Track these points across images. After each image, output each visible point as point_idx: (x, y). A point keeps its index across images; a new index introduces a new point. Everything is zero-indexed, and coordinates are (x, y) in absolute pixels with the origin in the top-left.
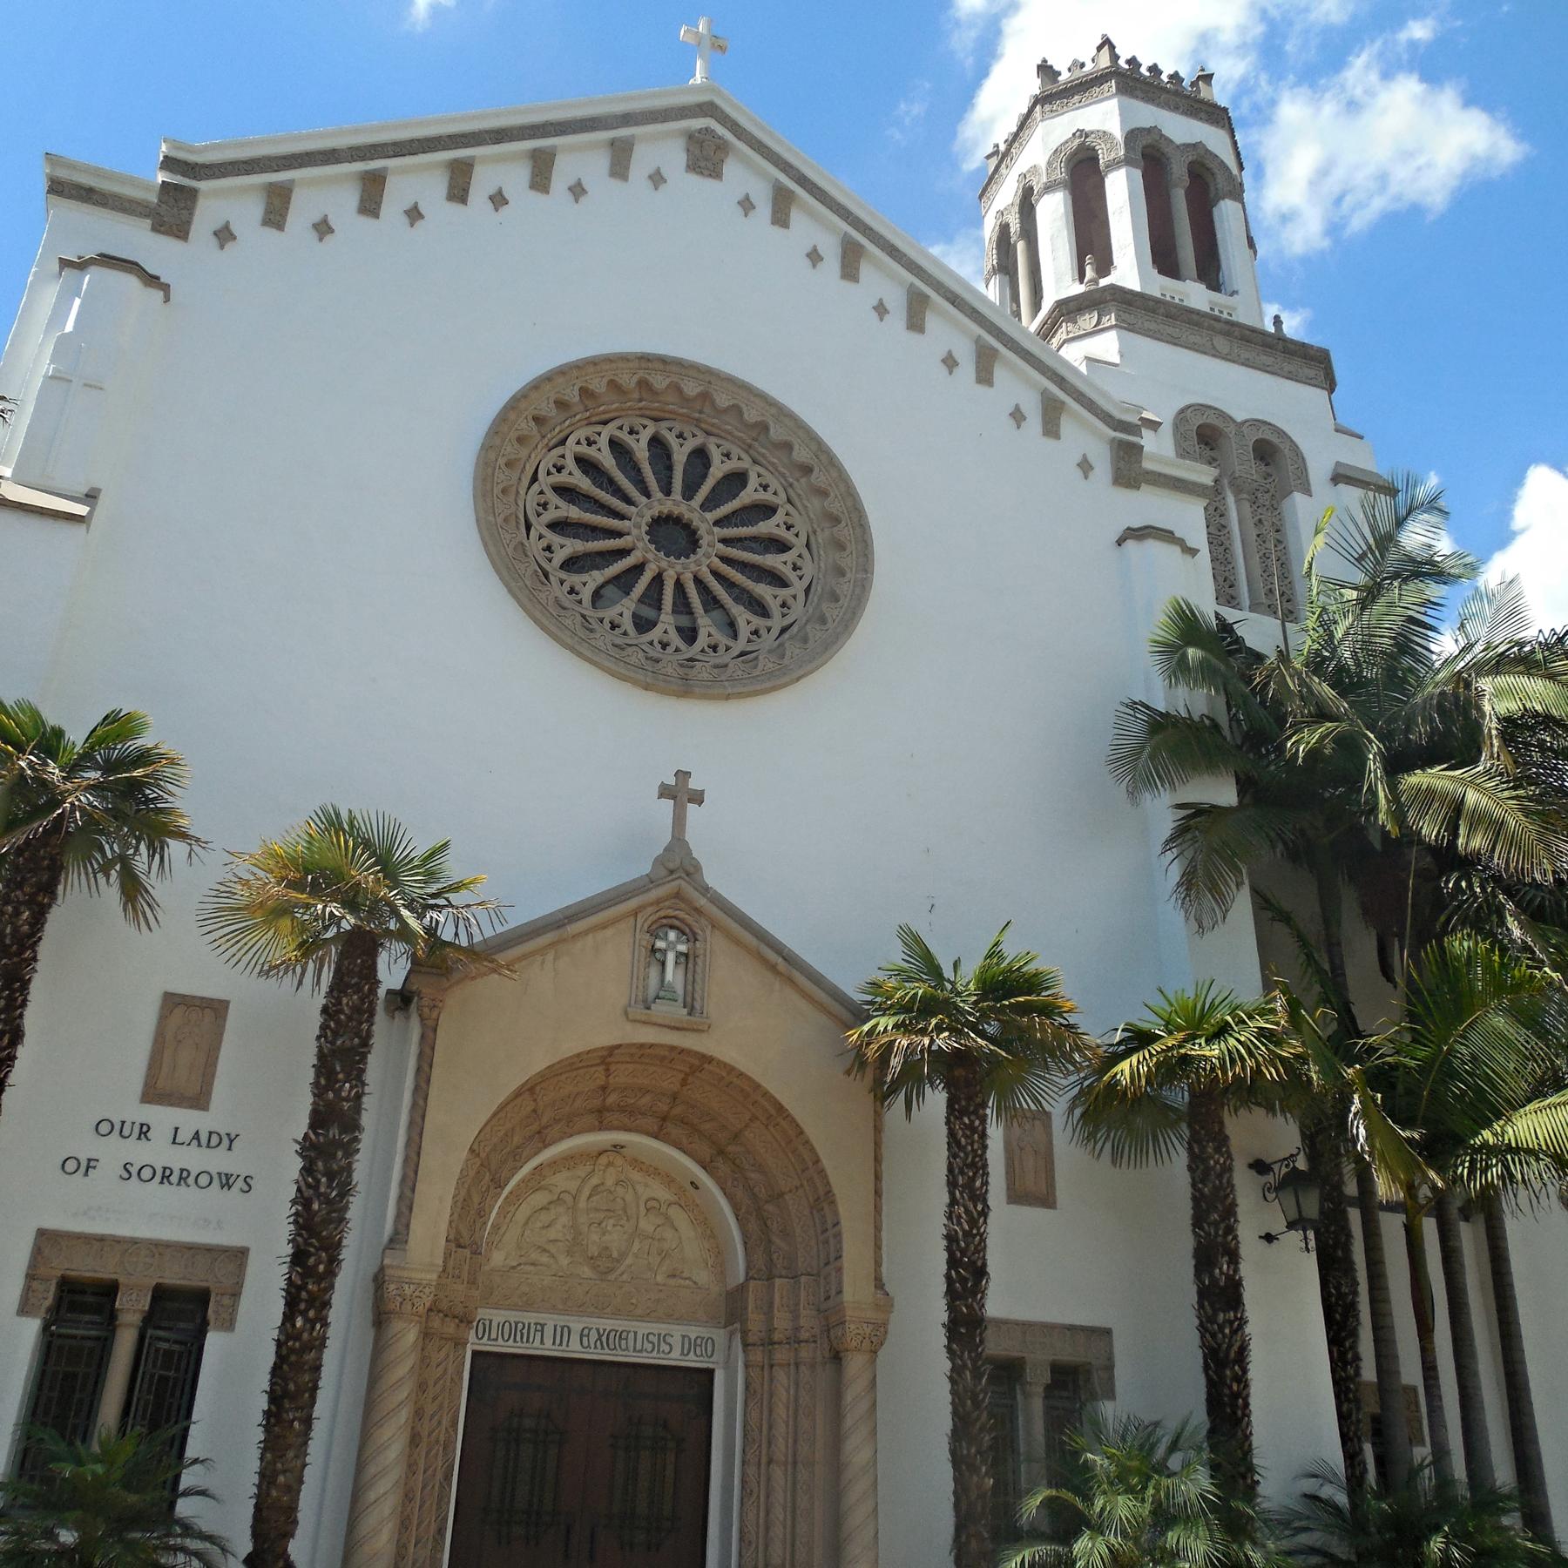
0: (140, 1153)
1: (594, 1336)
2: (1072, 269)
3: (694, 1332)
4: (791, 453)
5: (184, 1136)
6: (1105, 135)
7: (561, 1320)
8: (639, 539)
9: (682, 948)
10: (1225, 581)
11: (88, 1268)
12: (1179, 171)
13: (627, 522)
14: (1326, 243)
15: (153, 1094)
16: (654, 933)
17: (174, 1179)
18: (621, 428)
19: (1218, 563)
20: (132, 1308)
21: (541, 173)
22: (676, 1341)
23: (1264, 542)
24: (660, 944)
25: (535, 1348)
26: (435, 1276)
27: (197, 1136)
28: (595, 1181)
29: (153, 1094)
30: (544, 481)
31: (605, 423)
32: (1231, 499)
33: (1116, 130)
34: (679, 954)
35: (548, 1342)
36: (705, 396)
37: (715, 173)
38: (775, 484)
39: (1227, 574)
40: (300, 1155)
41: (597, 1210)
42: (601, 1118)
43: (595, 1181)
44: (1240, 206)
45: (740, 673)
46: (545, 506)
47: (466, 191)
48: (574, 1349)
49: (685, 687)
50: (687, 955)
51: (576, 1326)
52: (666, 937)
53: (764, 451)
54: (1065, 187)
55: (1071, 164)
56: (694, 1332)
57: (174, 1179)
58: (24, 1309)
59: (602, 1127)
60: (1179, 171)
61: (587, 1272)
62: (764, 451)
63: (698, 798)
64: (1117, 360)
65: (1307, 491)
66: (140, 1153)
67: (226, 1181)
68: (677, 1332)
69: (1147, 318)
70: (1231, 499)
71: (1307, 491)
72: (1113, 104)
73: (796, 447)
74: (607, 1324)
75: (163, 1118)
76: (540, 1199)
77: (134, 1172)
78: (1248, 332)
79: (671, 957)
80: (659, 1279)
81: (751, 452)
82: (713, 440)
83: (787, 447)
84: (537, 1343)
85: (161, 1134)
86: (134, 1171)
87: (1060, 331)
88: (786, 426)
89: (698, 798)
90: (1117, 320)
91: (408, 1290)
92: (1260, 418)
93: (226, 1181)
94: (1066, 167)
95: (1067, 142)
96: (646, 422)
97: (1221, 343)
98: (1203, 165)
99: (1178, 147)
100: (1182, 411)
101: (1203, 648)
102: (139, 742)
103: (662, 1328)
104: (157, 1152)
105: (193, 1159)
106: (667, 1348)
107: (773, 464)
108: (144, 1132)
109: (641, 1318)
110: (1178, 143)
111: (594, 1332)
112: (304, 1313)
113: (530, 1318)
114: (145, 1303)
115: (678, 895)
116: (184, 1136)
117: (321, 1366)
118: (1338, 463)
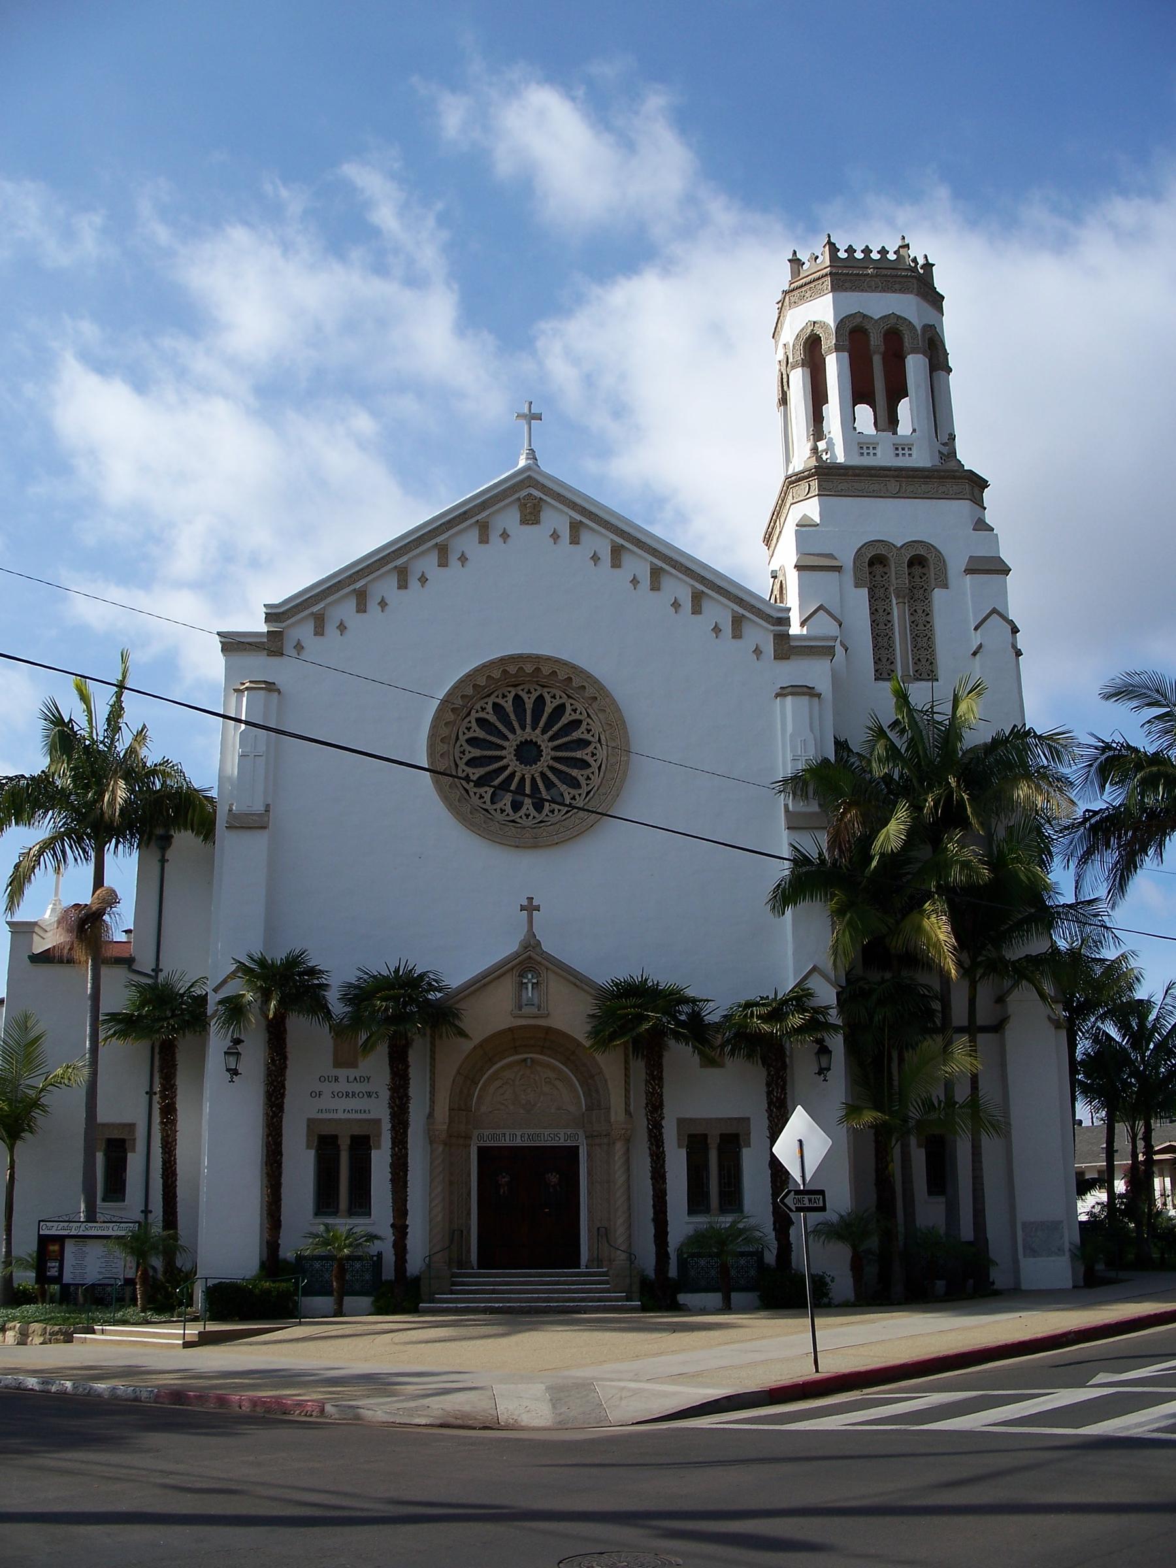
0: (336, 1087)
1: (526, 1136)
3: (569, 1132)
5: (351, 1079)
6: (824, 325)
7: (512, 1131)
8: (511, 760)
9: (535, 981)
11: (327, 1131)
12: (876, 340)
13: (505, 760)
14: (294, 1261)
15: (338, 1064)
16: (521, 976)
17: (350, 1096)
18: (497, 697)
20: (344, 1144)
21: (443, 553)
22: (562, 1136)
24: (525, 981)
25: (502, 1143)
26: (446, 1127)
27: (355, 1078)
28: (521, 1073)
29: (338, 1064)
30: (462, 738)
31: (489, 696)
33: (830, 319)
34: (533, 984)
35: (507, 1139)
36: (538, 670)
37: (537, 522)
38: (580, 708)
40: (389, 1089)
41: (523, 1085)
42: (516, 1050)
43: (521, 1073)
45: (562, 829)
46: (463, 753)
47: (406, 581)
48: (518, 1142)
49: (535, 845)
50: (537, 983)
51: (519, 1134)
52: (527, 978)
54: (803, 366)
55: (807, 346)
56: (569, 1132)
57: (350, 1096)
58: (308, 1147)
59: (517, 1053)
60: (876, 340)
61: (522, 1111)
63: (538, 909)
64: (819, 522)
66: (336, 1087)
67: (369, 1095)
68: (562, 1132)
69: (840, 481)
71: (946, 586)
72: (828, 299)
74: (531, 1131)
75: (342, 1073)
76: (498, 1083)
77: (336, 1094)
79: (530, 986)
80: (553, 1111)
82: (546, 690)
84: (503, 1141)
85: (342, 1079)
86: (336, 1094)
89: (538, 909)
91: (437, 1133)
93: (369, 1095)
95: (803, 329)
96: (509, 689)
97: (893, 486)
99: (876, 321)
102: (326, 993)
103: (556, 1131)
104: (343, 1086)
105: (357, 1087)
106: (558, 1139)
108: (336, 1079)
109: (545, 1128)
110: (876, 318)
111: (526, 1135)
112: (398, 1147)
113: (498, 1131)
114: (348, 1142)
115: (530, 957)
116: (351, 1079)
117: (750, 1133)
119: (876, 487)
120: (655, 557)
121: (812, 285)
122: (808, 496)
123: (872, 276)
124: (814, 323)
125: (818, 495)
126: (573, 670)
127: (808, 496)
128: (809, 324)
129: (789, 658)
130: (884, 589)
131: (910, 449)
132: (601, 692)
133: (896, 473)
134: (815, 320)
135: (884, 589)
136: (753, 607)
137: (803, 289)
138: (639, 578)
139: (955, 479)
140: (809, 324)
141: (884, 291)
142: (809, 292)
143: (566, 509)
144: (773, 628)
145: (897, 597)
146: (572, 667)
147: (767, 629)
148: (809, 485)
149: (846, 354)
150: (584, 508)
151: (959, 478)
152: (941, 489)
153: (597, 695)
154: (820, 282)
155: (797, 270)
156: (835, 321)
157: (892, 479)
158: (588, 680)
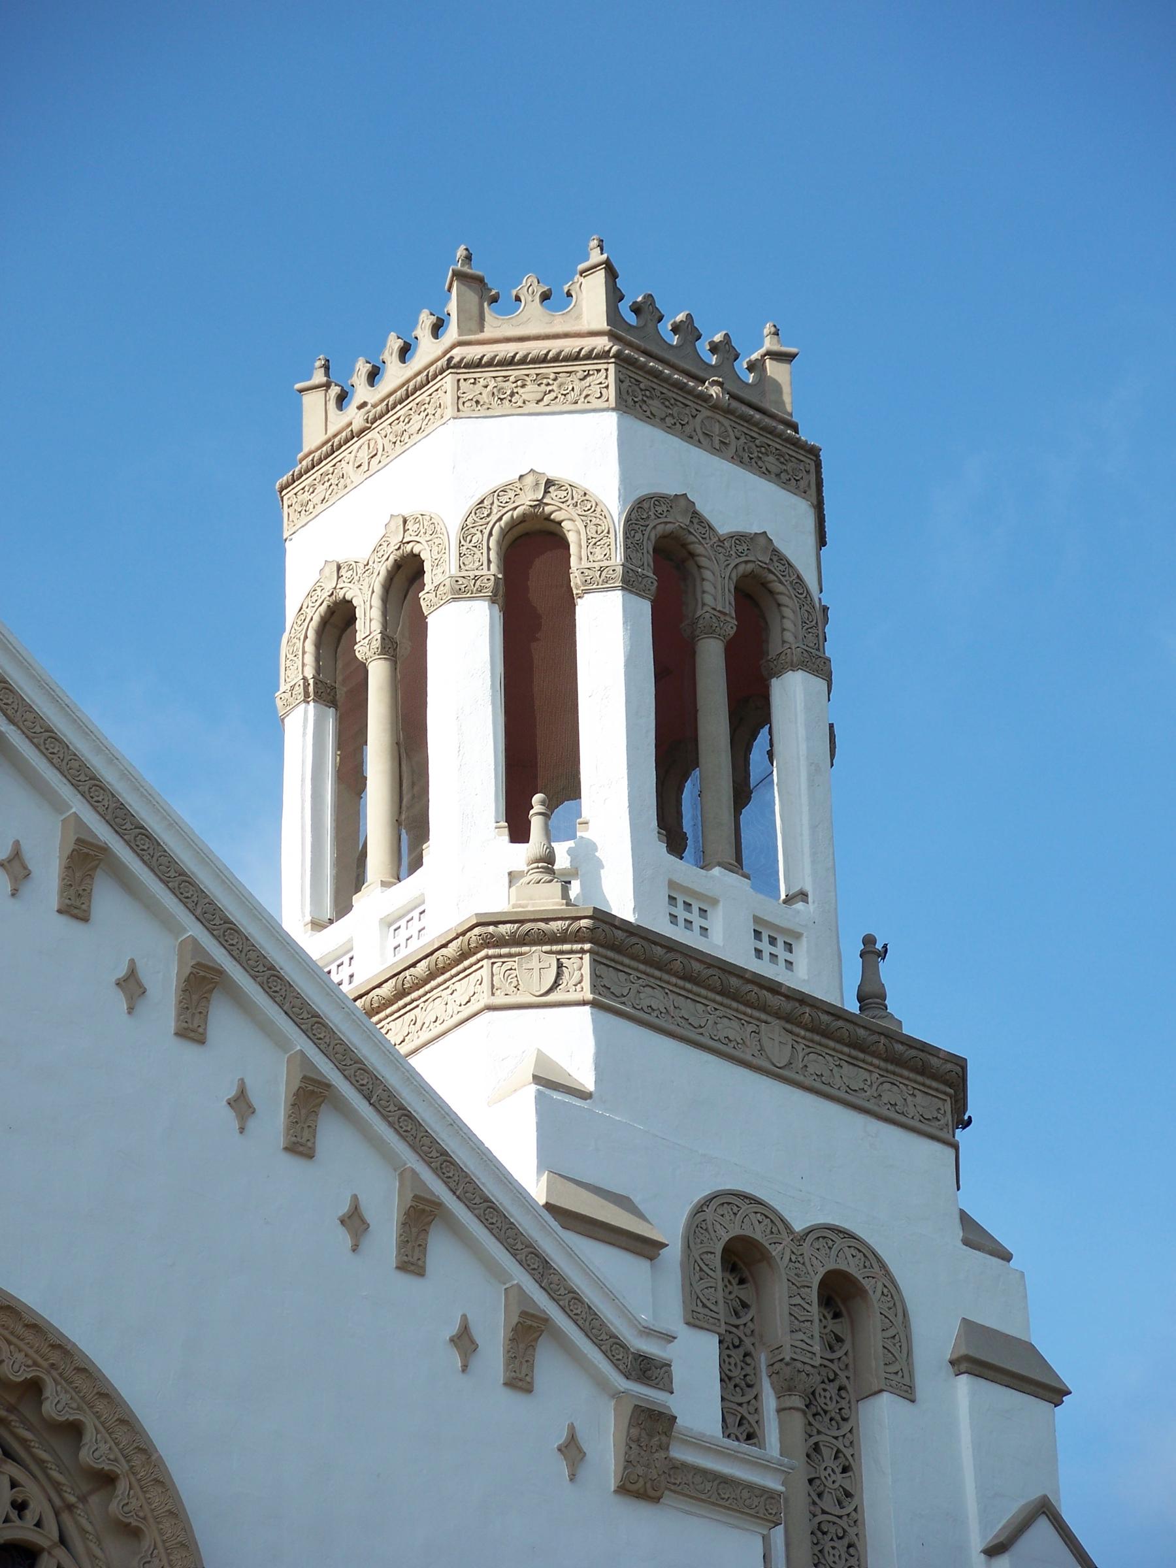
2: (493, 703)
4: (41, 1403)
6: (586, 503)
10: (740, 1424)
19: (731, 1386)
23: (820, 1495)
32: (769, 1402)
39: (743, 1410)
44: (824, 684)
53: (28, 1435)
55: (510, 537)
62: (28, 1435)
65: (908, 1393)
70: (769, 1402)
71: (908, 1393)
73: (89, 1435)
78: (825, 1018)
81: (65, 1517)
83: (74, 1430)
87: (477, 975)
88: (76, 1389)
90: (594, 988)
92: (836, 1222)
94: (499, 543)
98: (764, 585)
100: (700, 1209)
101: (592, 943)
107: (40, 1462)
118: (968, 1326)
119: (730, 1029)
120: (316, 1041)
121: (549, 370)
122: (552, 997)
123: (716, 407)
124: (549, 483)
125: (594, 1004)
126: (55, 1357)
127: (552, 997)
128: (529, 480)
129: (656, 1500)
130: (741, 1351)
131: (789, 947)
132: (138, 1460)
133: (788, 1006)
134: (552, 474)
135: (741, 1351)
136: (577, 1298)
137: (514, 374)
138: (254, 1097)
139: (922, 1073)
140: (529, 480)
141: (739, 459)
142: (531, 387)
143: (66, 791)
144: (622, 1383)
145: (784, 1390)
146: (54, 1346)
147: (601, 1383)
148: (560, 966)
149: (645, 607)
150: (122, 806)
151: (934, 1077)
152: (890, 1094)
153: (121, 1468)
154: (579, 368)
155: (475, 310)
156: (623, 497)
157: (775, 1022)
158: (100, 1406)
